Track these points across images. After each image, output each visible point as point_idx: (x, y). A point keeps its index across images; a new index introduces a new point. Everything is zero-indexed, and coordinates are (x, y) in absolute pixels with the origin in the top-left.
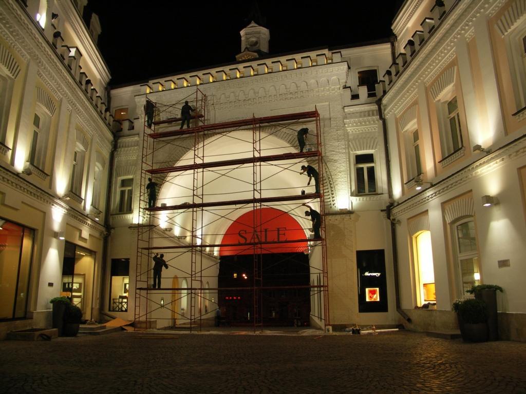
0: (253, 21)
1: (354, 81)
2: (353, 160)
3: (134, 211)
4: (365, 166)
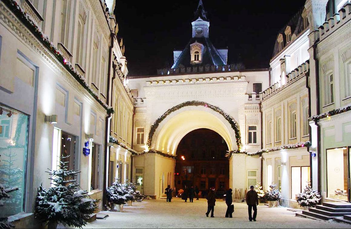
0: (199, 17)
1: (251, 90)
2: (247, 128)
3: (231, 188)
4: (252, 131)
